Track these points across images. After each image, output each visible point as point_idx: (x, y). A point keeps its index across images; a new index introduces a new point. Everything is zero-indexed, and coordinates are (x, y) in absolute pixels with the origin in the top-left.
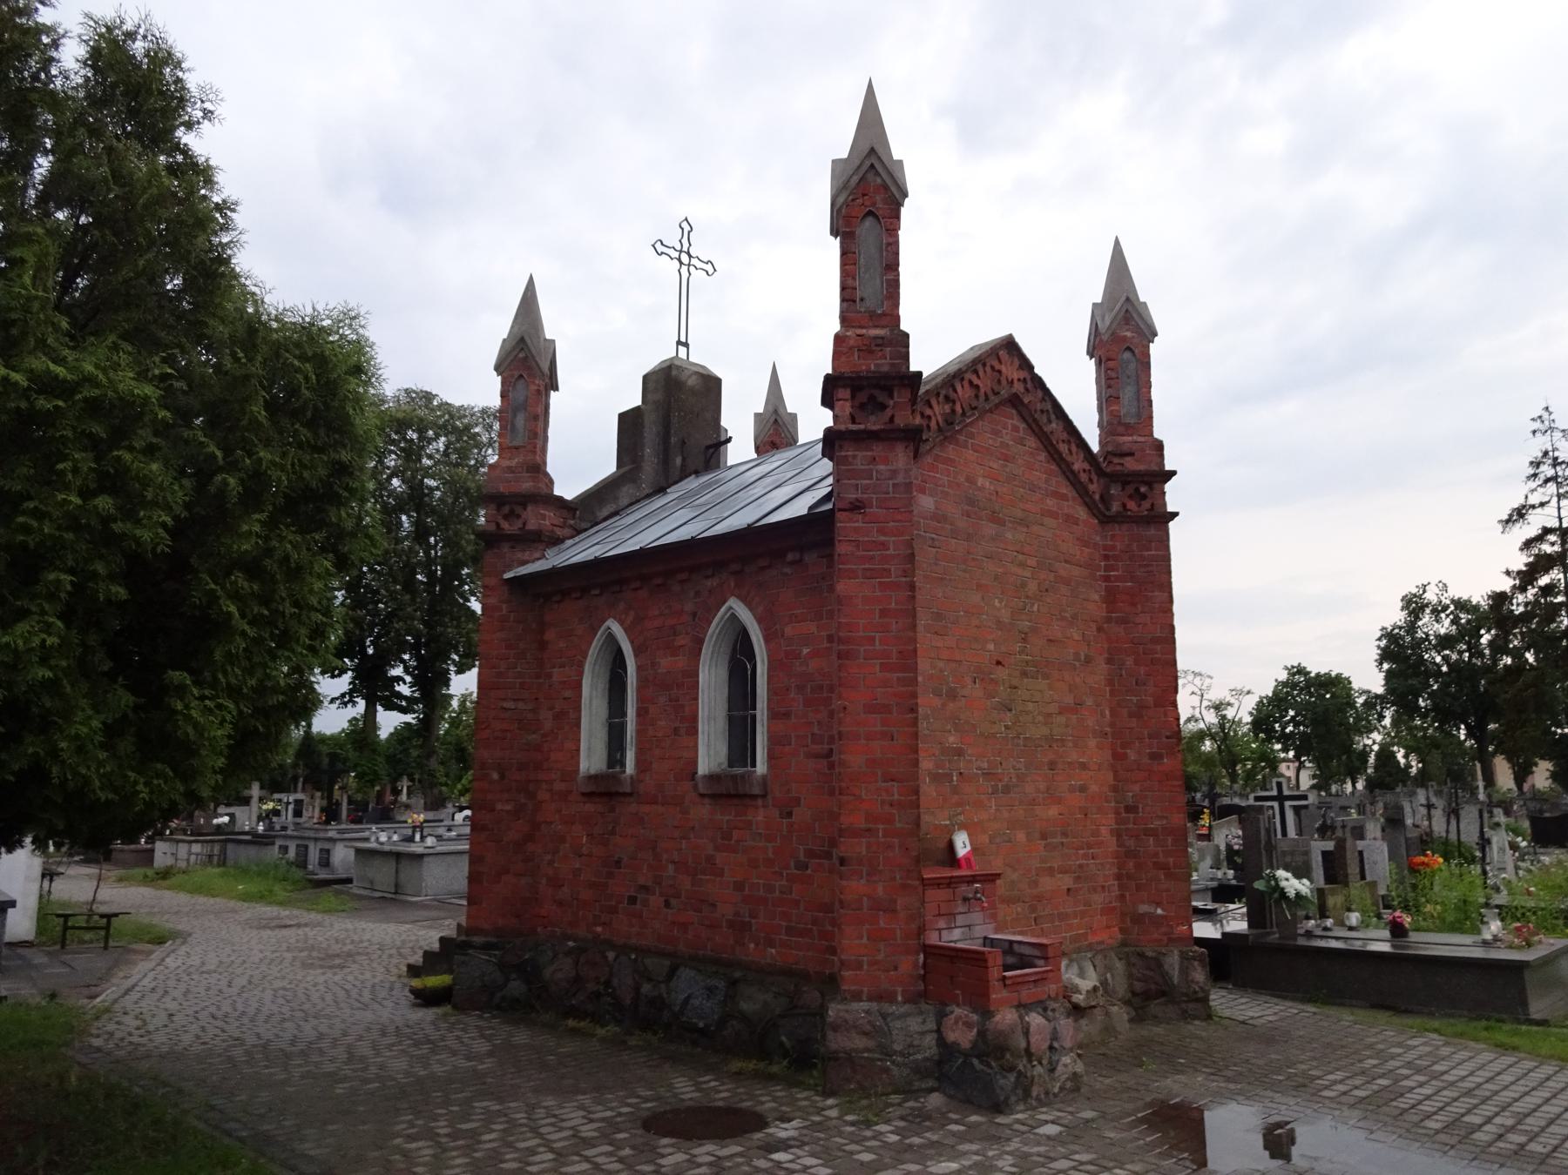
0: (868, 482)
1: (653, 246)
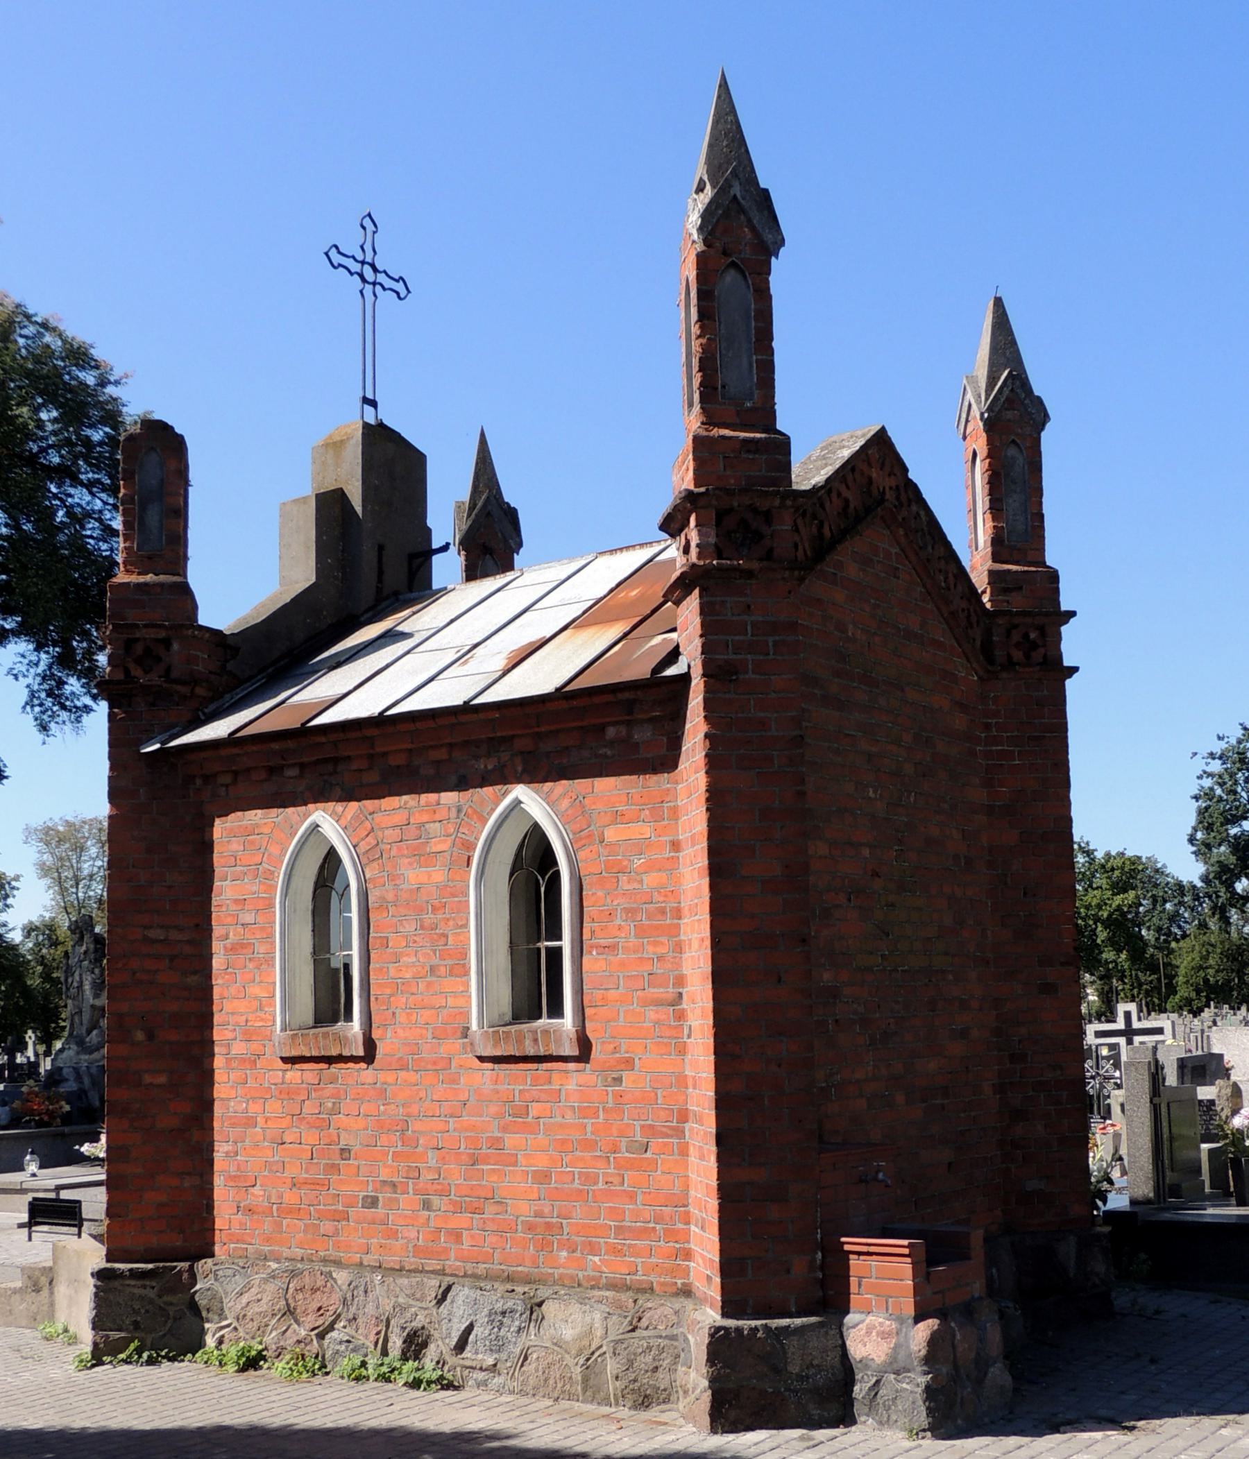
0: (741, 638)
1: (326, 254)
